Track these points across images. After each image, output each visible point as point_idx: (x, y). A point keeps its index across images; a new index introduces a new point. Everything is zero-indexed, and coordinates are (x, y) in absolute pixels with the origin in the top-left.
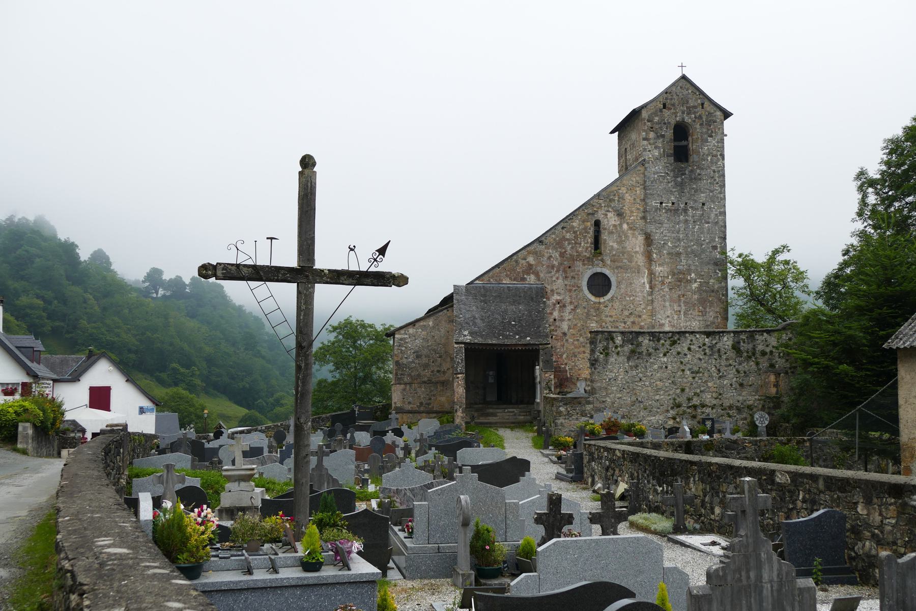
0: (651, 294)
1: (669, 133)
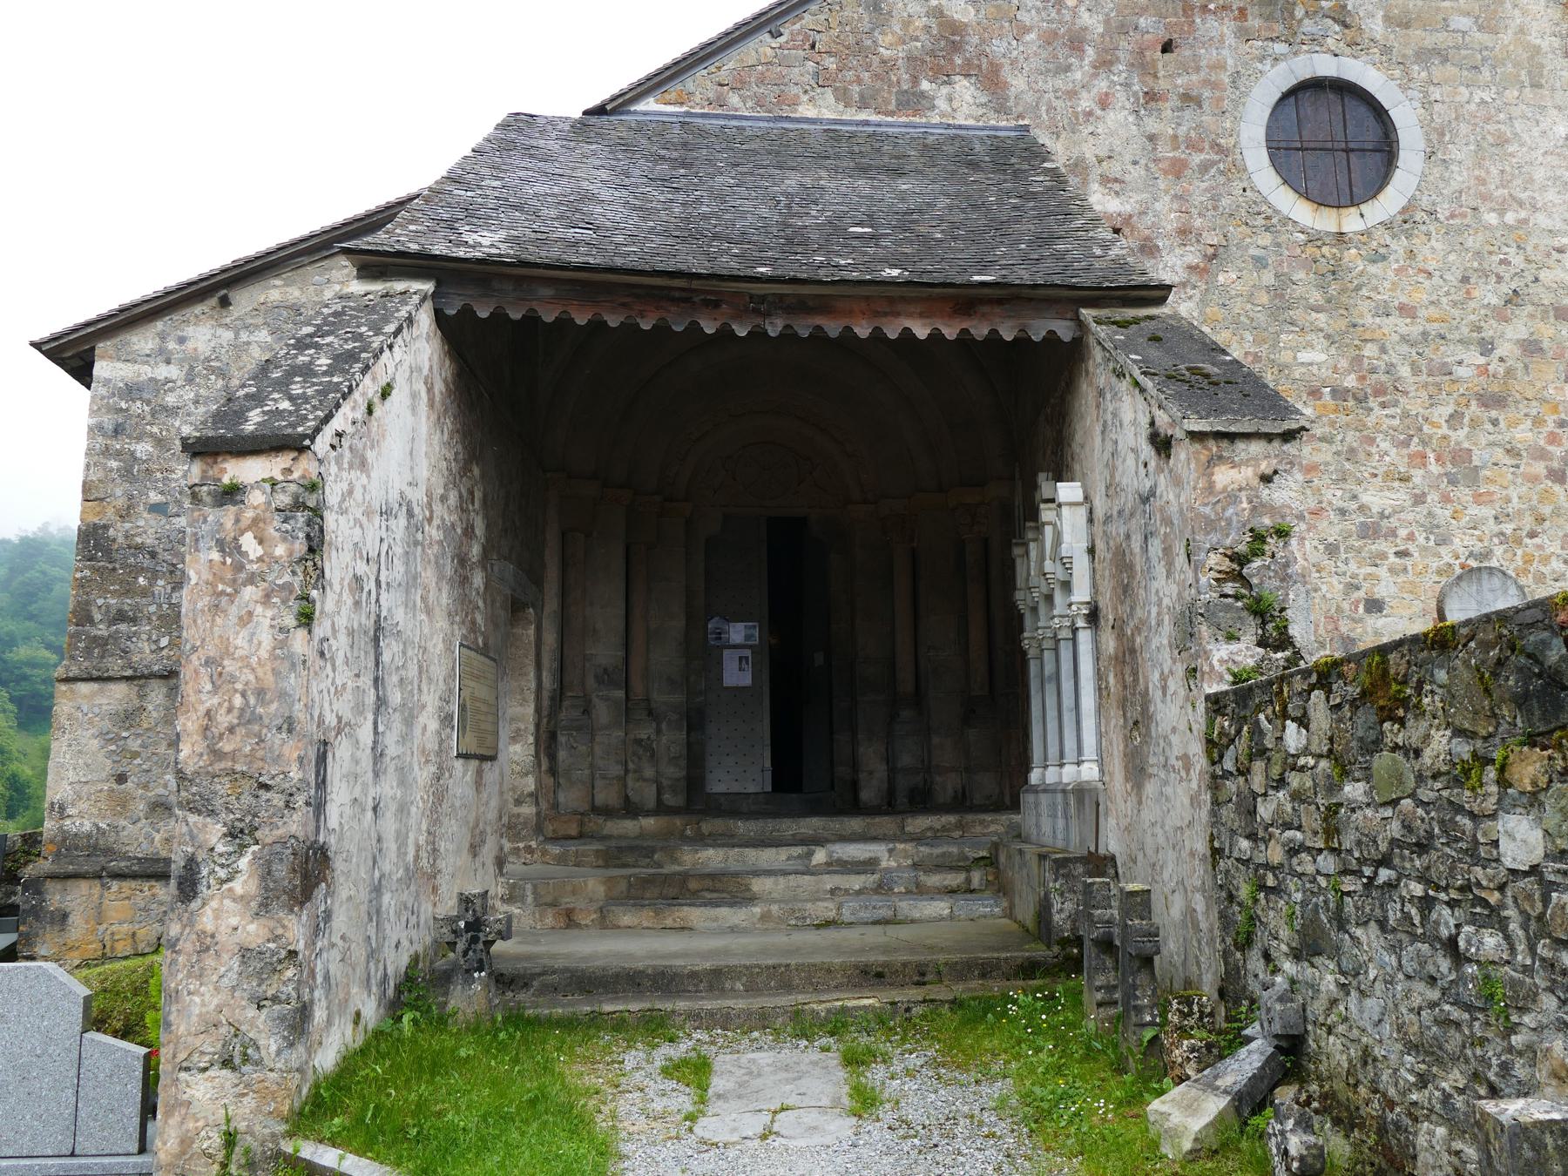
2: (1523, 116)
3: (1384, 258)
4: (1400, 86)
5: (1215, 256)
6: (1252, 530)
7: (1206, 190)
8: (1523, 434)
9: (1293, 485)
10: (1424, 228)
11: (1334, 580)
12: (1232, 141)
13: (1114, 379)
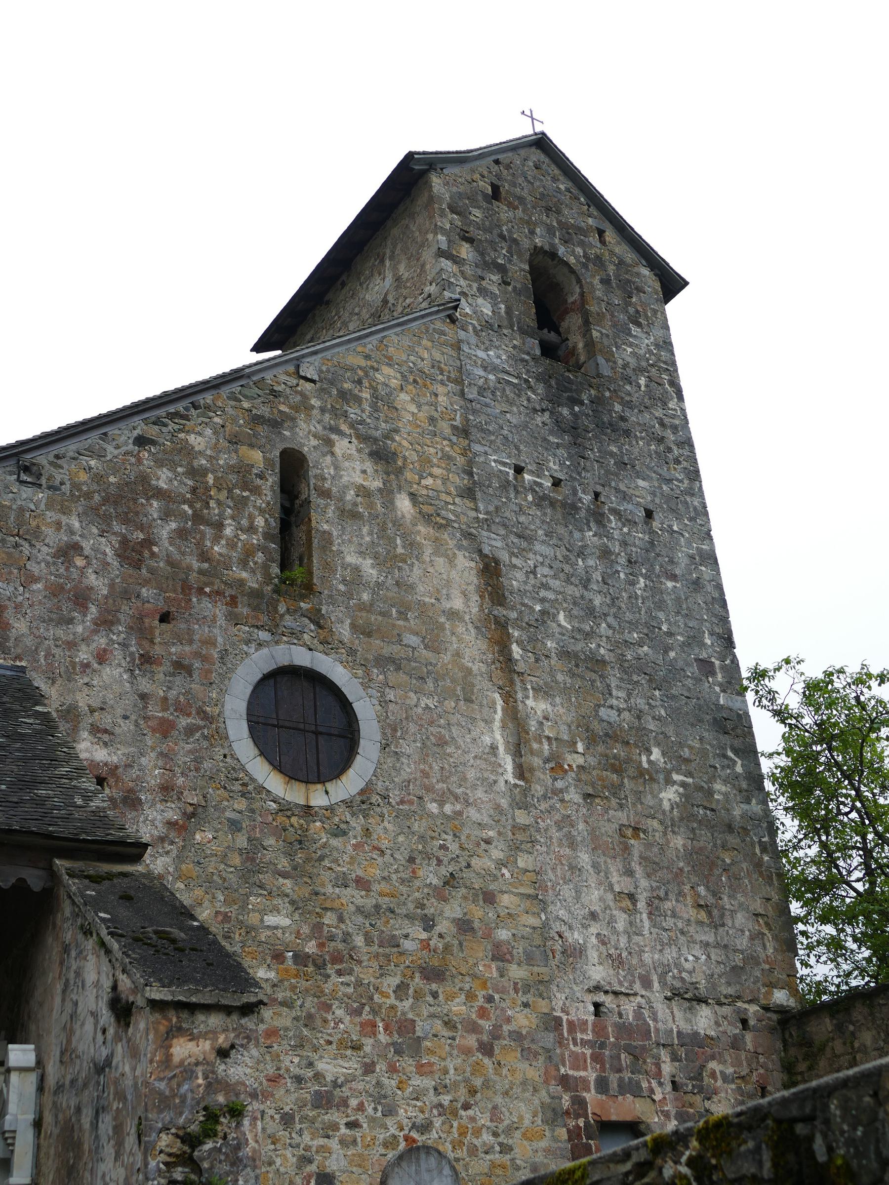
0: (522, 800)
1: (519, 269)
2: (459, 724)
3: (344, 833)
4: (362, 684)
5: (194, 815)
6: (205, 1109)
7: (190, 752)
8: (458, 1007)
9: (247, 1060)
10: (378, 810)
11: (288, 1153)
12: (217, 710)
13: (80, 936)
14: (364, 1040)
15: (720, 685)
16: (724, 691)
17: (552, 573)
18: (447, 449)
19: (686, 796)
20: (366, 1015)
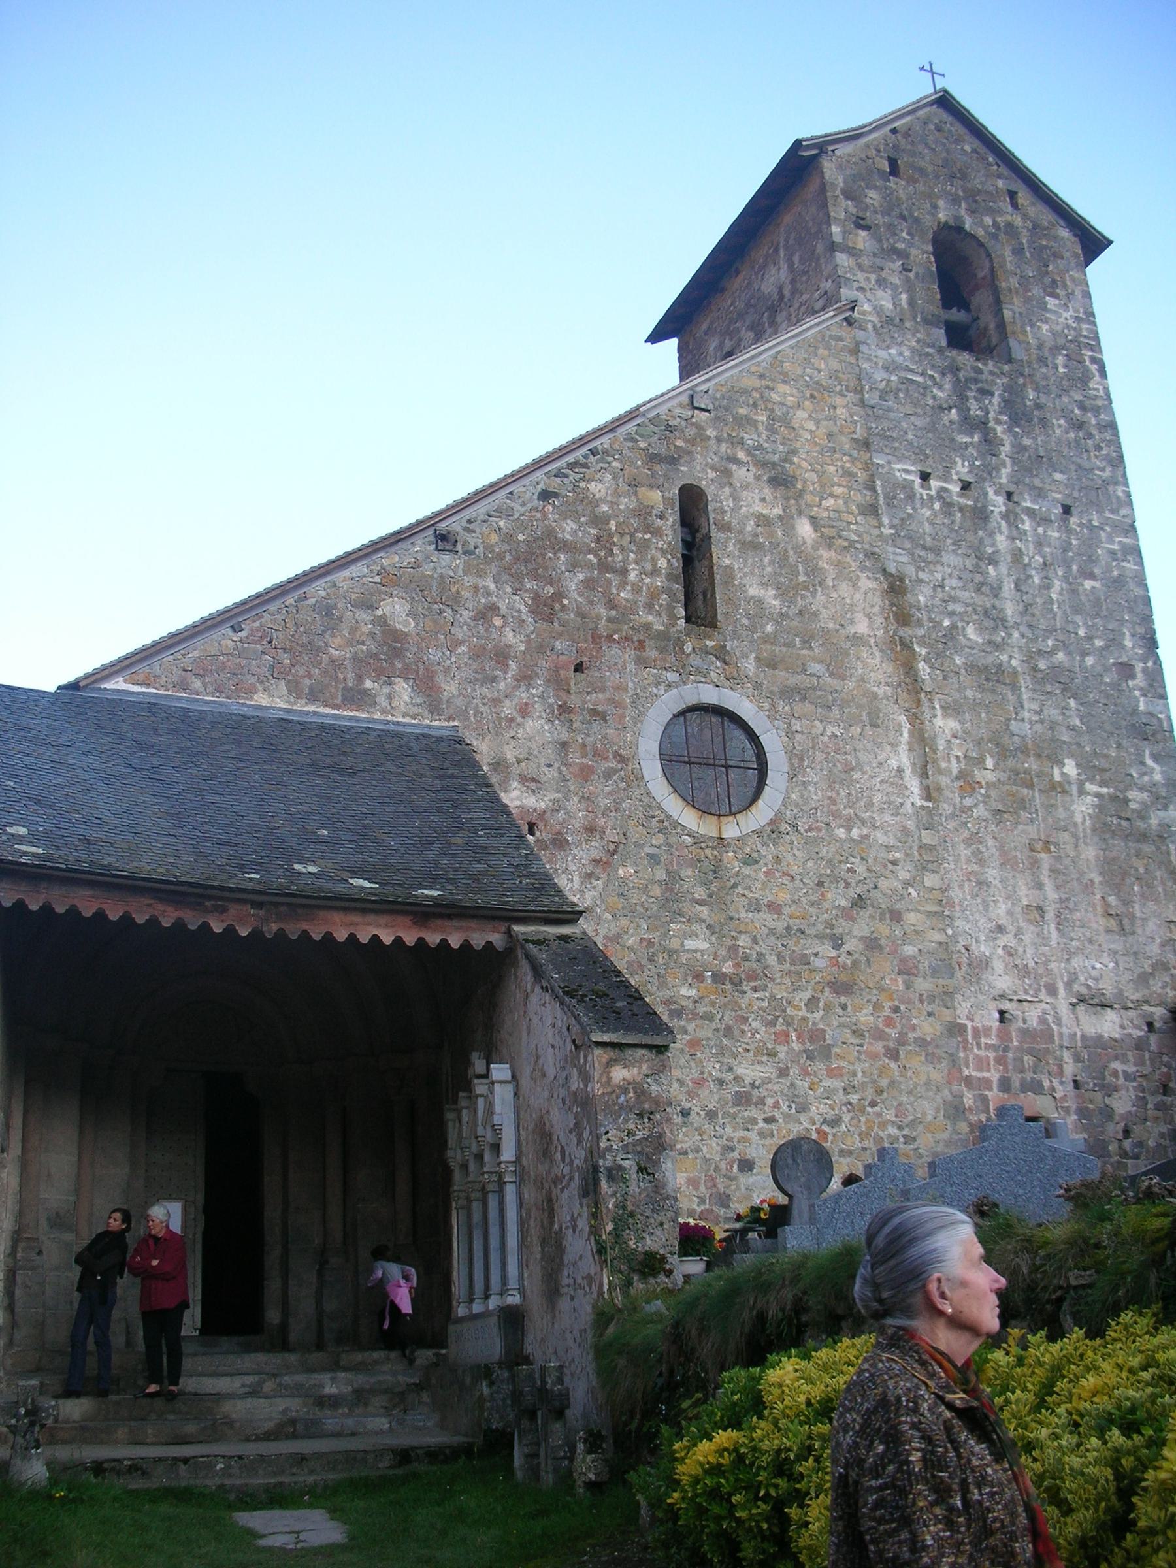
0: (928, 819)
1: (922, 255)
2: (865, 750)
3: (756, 862)
4: (768, 717)
8: (865, 1017)
14: (778, 1048)
15: (1141, 689)
16: (1145, 695)
17: (960, 584)
18: (848, 465)
19: (1100, 808)
20: (779, 1027)
